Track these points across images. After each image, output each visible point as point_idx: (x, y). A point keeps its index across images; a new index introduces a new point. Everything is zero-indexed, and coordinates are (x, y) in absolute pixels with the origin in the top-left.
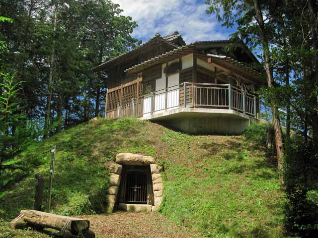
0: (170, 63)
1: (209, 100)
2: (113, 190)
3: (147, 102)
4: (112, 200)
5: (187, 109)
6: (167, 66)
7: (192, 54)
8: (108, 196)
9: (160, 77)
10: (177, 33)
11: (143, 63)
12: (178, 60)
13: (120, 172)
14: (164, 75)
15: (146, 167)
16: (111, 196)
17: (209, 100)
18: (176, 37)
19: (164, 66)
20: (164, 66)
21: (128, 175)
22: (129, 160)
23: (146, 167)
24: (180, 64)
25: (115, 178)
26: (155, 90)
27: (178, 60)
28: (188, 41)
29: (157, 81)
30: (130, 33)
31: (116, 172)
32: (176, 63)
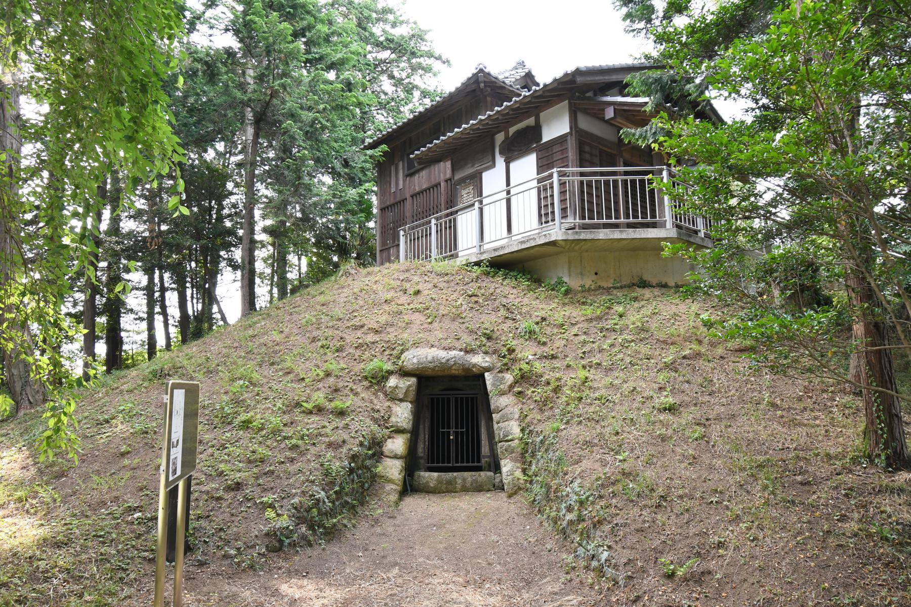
0: (512, 130)
1: (608, 209)
2: (397, 445)
3: (466, 222)
4: (393, 469)
5: (556, 232)
6: (507, 137)
7: (566, 102)
8: (622, 3)
9: (493, 165)
10: (522, 64)
11: (423, 149)
12: (531, 121)
13: (412, 395)
14: (500, 162)
15: (476, 378)
16: (388, 462)
17: (608, 209)
18: (521, 73)
19: (500, 138)
20: (500, 138)
21: (432, 399)
22: (431, 365)
23: (476, 378)
24: (535, 132)
25: (402, 414)
26: (481, 195)
27: (531, 121)
28: (545, 77)
29: (487, 176)
30: (155, 36)
31: (401, 396)
32: (528, 128)
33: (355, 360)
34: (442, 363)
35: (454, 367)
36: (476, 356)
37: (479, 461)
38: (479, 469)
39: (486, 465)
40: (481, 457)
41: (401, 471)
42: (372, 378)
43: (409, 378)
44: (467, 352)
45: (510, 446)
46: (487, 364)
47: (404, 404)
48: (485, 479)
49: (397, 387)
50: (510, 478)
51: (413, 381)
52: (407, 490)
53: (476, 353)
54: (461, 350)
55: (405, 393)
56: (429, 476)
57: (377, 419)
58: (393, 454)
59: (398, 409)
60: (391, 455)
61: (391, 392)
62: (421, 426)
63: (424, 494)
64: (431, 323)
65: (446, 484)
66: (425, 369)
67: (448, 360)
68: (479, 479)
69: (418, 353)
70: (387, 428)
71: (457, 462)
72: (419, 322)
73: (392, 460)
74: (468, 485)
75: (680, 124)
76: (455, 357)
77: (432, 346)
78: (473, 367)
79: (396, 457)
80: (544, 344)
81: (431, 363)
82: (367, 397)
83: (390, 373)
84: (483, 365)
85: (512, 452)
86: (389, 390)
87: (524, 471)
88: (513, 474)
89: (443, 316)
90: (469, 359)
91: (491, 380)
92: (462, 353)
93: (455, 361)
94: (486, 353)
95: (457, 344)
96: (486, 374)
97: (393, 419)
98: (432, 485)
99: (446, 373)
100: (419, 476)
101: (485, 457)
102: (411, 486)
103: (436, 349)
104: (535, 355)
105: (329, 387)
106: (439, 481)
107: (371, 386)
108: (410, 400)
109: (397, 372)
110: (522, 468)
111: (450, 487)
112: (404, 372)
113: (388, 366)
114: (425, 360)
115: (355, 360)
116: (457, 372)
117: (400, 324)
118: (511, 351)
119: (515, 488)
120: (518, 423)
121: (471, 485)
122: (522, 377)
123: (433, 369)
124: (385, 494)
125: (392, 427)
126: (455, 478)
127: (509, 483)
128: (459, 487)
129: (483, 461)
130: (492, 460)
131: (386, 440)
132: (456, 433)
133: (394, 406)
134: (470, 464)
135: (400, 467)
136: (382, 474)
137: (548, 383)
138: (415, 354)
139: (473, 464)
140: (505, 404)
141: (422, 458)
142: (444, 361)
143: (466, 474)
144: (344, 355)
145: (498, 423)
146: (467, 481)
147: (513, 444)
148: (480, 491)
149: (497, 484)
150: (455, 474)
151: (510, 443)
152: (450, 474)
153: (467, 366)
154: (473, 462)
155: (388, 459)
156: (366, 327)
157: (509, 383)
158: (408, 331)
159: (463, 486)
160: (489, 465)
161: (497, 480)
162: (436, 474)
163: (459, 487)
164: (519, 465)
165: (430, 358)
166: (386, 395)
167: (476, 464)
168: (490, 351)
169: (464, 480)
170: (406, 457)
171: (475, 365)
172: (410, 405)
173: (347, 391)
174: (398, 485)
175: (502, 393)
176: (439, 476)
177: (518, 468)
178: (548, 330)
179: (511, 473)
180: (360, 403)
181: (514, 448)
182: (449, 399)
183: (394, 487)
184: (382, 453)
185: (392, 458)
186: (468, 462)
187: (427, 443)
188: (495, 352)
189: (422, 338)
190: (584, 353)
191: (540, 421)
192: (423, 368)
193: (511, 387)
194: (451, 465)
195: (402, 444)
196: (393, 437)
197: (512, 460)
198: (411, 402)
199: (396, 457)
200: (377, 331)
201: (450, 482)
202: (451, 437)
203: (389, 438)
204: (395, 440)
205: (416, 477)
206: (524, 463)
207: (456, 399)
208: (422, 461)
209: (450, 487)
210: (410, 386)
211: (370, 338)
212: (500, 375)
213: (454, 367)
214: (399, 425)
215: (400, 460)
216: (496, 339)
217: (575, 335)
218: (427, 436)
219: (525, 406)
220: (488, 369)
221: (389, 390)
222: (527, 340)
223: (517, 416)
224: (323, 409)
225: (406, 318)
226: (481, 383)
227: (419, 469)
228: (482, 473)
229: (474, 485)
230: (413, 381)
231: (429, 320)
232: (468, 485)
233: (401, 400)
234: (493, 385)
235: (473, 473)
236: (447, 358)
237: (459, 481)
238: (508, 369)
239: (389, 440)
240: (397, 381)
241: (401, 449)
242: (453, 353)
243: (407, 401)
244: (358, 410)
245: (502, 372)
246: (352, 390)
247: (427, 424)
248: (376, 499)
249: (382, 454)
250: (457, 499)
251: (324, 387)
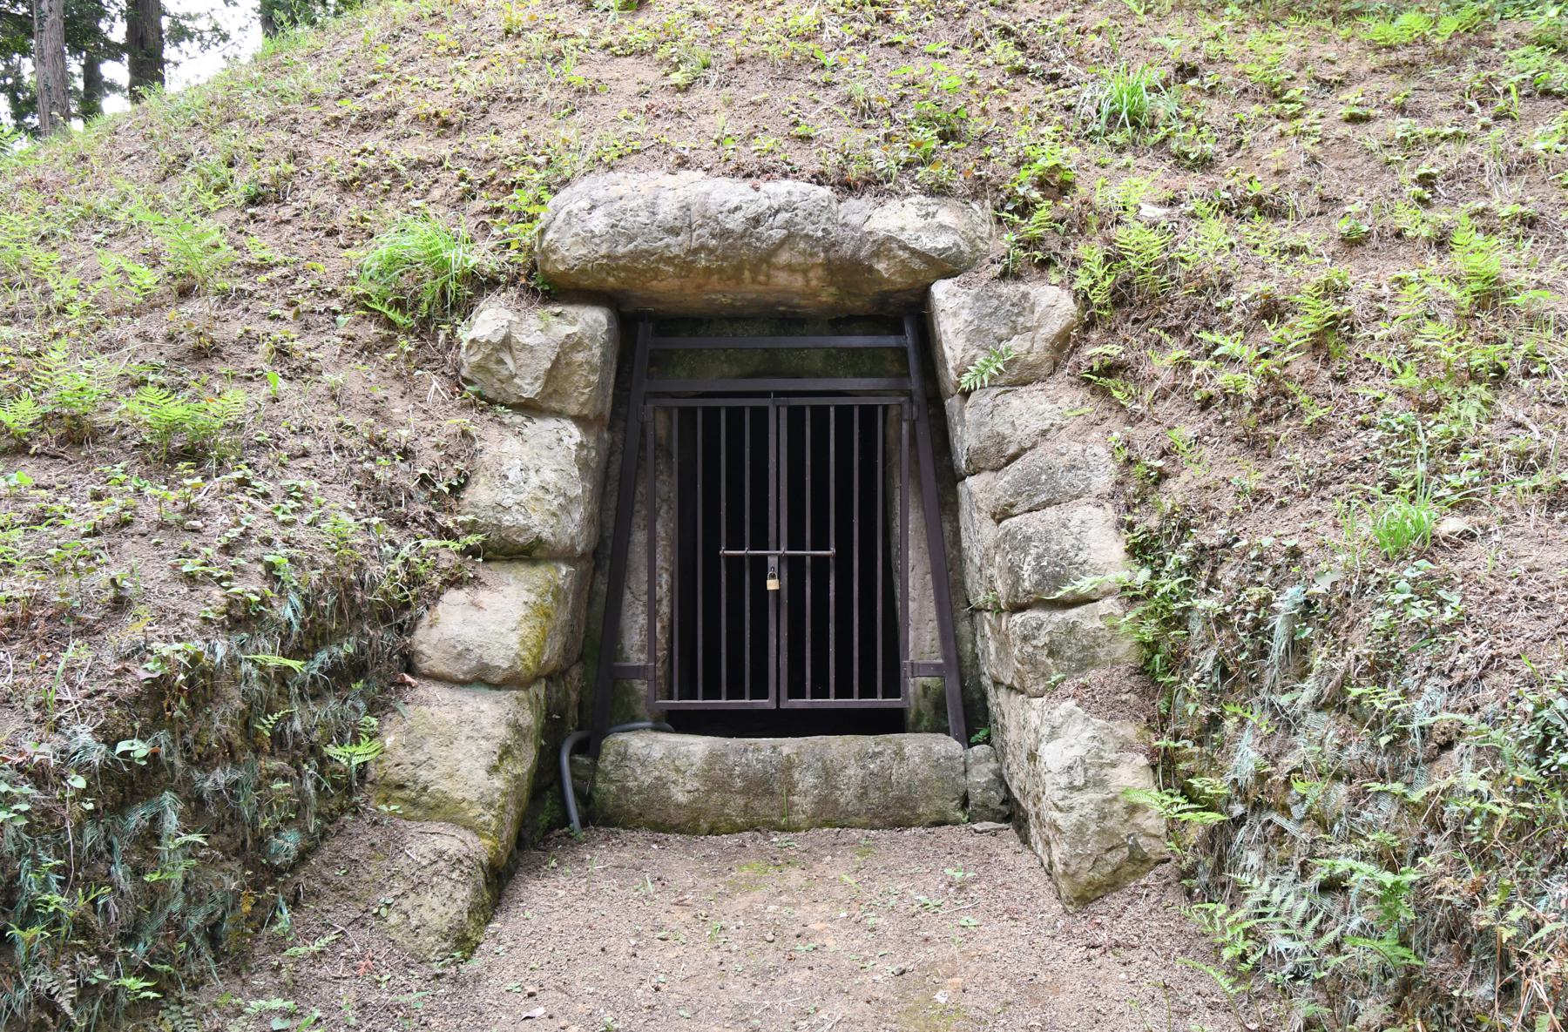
13: (585, 387)
22: (676, 245)
31: (529, 388)
33: (332, 233)
34: (725, 234)
35: (784, 257)
36: (893, 204)
37: (893, 688)
38: (892, 722)
39: (926, 706)
40: (905, 668)
41: (506, 752)
42: (399, 305)
43: (571, 311)
44: (847, 187)
45: (1072, 628)
46: (943, 241)
47: (543, 429)
48: (924, 771)
49: (506, 343)
50: (1087, 801)
51: (591, 320)
52: (565, 820)
53: (892, 194)
54: (819, 179)
55: (552, 374)
56: (670, 755)
57: (393, 489)
58: (470, 664)
59: (512, 445)
60: (459, 670)
61: (480, 367)
62: (639, 537)
63: (640, 836)
64: (686, 89)
65: (744, 792)
66: (644, 263)
67: (756, 221)
68: (898, 772)
69: (614, 192)
70: (446, 533)
71: (796, 691)
72: (631, 87)
73: (459, 694)
74: (847, 796)
75: (626, 776)
76: (790, 207)
77: (683, 163)
78: (876, 254)
79: (481, 679)
80: (1205, 164)
81: (673, 231)
82: (356, 387)
83: (482, 284)
84: (928, 243)
85: (1086, 662)
86: (469, 359)
87: (1165, 767)
88: (1100, 783)
89: (740, 62)
90: (855, 220)
91: (965, 315)
92: (825, 192)
93: (788, 224)
94: (939, 191)
95: (804, 159)
96: (941, 290)
97: (480, 494)
98: (681, 797)
99: (750, 289)
100: (624, 756)
101: (917, 670)
102: (585, 799)
103: (700, 173)
104: (1173, 202)
105: (170, 338)
106: (715, 778)
107: (388, 343)
108: (574, 409)
109: (513, 282)
110: (1154, 752)
111: (762, 806)
112: (549, 279)
113: (480, 257)
114: (643, 218)
115: (332, 233)
116: (798, 282)
117: (546, 95)
118: (1055, 185)
119: (1116, 858)
120: (1110, 511)
121: (863, 795)
122: (1119, 298)
123: (685, 265)
124: (400, 886)
125: (472, 528)
126: (788, 766)
127: (1080, 828)
128: (804, 804)
129: (914, 685)
130: (953, 686)
131: (436, 596)
132: (794, 567)
133: (494, 432)
134: (855, 702)
135: (502, 732)
136: (396, 775)
137: (1272, 310)
138: (600, 194)
139: (868, 702)
140: (1036, 425)
141: (638, 672)
142: (735, 223)
143: (838, 746)
144: (286, 213)
145: (1000, 516)
146: (842, 780)
147: (1087, 619)
148: (901, 824)
149: (977, 796)
150: (789, 746)
151: (1072, 614)
152: (765, 742)
153: (847, 249)
154: (867, 691)
155: (438, 692)
156: (403, 115)
157: (1054, 326)
158: (580, 117)
159: (822, 801)
160: (940, 705)
161: (981, 776)
162: (698, 746)
163: (804, 804)
164: (1130, 730)
165: (668, 210)
166: (458, 382)
167: (879, 701)
168: (959, 183)
169: (828, 774)
170: (552, 677)
171: (884, 247)
172: (573, 434)
173: (260, 359)
174: (478, 831)
175: (1020, 377)
176: (714, 757)
177: (1125, 746)
178: (1217, 111)
179: (1092, 774)
180: (325, 419)
181: (1095, 639)
182: (760, 415)
183: (453, 842)
184: (409, 662)
185: (463, 684)
186: (844, 691)
187: (664, 609)
188: (979, 188)
189: (638, 137)
190: (1426, 180)
191: (1260, 497)
192: (635, 256)
193: (1064, 345)
194: (767, 703)
195: (519, 612)
196: (475, 581)
197: (1091, 701)
198: (579, 420)
199: (481, 679)
200: (446, 124)
201: (761, 785)
202: (772, 585)
203: (455, 582)
204: (483, 596)
205: (607, 761)
206: (1158, 723)
207: (796, 415)
208: (641, 687)
209: (762, 806)
210: (571, 345)
211: (420, 147)
212: (1008, 289)
213: (784, 257)
214: (507, 520)
215: (508, 699)
216: (983, 140)
217: (1353, 119)
218: (664, 579)
219: (1139, 433)
220: (949, 266)
221: (469, 359)
222: (1121, 150)
223: (1103, 481)
224: (96, 435)
225: (578, 75)
226: (909, 340)
227: (628, 720)
228: (912, 744)
229: (875, 796)
230: (591, 320)
231: (677, 78)
232: (847, 796)
233: (530, 409)
234: (977, 335)
235: (869, 742)
236: (751, 211)
237: (806, 780)
238: (1045, 264)
239: (452, 596)
240: (509, 315)
241: (513, 640)
242: (778, 190)
243: (559, 414)
244: (293, 443)
245: (1017, 277)
246: (282, 353)
247: (665, 528)
248: (341, 915)
249: (410, 669)
250: (795, 877)
251: (143, 336)
